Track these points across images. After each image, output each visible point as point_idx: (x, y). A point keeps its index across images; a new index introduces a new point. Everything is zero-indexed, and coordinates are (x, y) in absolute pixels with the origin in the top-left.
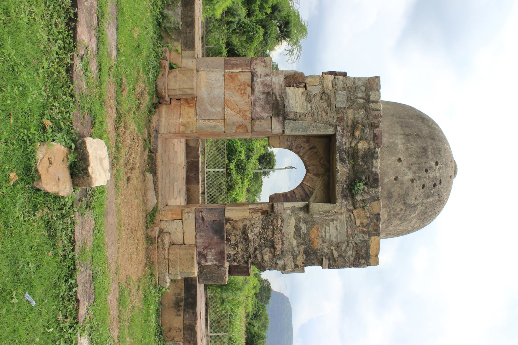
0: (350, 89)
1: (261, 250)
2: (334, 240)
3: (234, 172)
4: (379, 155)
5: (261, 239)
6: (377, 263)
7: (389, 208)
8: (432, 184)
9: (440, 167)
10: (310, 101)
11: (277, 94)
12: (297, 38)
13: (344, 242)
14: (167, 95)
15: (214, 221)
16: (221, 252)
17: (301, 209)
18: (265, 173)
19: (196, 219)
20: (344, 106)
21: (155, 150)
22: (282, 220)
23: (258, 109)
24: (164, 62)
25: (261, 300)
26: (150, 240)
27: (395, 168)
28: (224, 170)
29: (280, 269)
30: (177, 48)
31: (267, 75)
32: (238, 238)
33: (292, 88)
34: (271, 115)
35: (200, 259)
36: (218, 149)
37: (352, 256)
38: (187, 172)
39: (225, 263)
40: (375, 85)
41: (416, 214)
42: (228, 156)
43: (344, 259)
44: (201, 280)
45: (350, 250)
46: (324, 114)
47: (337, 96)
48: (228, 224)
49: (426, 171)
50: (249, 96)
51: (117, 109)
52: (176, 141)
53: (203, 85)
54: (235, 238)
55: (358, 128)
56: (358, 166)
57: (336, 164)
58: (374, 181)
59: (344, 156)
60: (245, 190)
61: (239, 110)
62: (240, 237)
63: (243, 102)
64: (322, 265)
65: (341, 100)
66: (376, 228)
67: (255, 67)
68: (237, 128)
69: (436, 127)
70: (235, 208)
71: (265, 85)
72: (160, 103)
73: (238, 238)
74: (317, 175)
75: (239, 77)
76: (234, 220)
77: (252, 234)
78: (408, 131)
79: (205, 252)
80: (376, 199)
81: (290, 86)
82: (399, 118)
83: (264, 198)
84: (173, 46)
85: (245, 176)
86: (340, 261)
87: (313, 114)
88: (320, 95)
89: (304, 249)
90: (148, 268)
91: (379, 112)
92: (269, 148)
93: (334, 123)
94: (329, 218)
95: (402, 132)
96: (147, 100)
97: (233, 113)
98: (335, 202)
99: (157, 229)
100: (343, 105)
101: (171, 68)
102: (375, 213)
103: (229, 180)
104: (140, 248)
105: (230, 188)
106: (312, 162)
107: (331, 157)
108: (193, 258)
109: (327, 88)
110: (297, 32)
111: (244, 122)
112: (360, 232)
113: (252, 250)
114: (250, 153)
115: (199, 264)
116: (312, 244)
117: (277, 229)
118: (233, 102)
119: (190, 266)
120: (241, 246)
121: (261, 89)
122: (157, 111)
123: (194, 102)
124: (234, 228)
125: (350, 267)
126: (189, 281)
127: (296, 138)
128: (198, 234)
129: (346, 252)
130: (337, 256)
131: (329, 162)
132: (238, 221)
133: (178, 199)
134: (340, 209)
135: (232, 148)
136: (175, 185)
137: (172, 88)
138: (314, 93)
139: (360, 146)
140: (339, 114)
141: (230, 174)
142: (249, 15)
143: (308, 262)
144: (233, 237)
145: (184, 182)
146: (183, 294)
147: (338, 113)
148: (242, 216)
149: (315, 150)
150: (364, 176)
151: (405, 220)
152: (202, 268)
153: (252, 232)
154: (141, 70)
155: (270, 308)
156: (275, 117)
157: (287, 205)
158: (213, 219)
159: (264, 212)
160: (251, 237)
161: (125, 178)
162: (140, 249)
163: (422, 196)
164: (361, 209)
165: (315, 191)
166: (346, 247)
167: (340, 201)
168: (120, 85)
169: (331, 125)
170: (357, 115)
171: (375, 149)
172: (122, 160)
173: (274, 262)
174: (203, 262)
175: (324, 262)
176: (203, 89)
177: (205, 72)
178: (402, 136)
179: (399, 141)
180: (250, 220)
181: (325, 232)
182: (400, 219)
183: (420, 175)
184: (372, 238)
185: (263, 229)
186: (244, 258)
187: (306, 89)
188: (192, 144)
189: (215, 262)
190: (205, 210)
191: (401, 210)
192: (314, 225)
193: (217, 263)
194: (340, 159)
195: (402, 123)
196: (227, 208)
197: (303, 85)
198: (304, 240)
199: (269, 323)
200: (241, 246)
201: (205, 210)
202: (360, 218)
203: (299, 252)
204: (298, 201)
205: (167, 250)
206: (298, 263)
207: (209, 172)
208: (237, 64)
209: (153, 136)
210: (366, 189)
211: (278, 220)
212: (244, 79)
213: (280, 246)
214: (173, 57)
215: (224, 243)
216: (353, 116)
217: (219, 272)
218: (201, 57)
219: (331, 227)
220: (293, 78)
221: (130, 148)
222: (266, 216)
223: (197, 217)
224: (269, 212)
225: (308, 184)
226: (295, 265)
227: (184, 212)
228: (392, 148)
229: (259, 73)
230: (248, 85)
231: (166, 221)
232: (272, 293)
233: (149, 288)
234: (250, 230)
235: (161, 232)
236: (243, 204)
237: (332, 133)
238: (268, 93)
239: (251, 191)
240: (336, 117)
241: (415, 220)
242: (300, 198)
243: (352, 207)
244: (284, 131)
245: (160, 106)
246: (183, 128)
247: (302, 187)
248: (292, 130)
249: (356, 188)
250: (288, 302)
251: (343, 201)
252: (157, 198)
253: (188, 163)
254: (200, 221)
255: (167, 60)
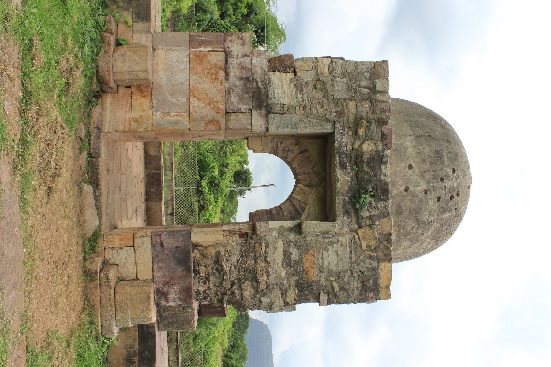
0: (351, 76)
1: (240, 284)
2: (334, 268)
3: (206, 190)
4: (389, 159)
5: (239, 269)
6: (388, 296)
7: (399, 226)
8: (449, 196)
9: (457, 175)
10: (301, 90)
11: (259, 80)
12: (275, 44)
13: (347, 271)
14: (111, 79)
15: (177, 247)
16: (187, 289)
17: (291, 229)
18: (241, 193)
19: (153, 245)
20: (344, 96)
21: (96, 153)
22: (267, 244)
23: (234, 99)
24: (107, 35)
25: (239, 330)
26: (88, 275)
27: (405, 176)
28: (195, 187)
29: (265, 308)
30: (126, 19)
31: (246, 55)
32: (209, 269)
33: (277, 74)
34: (250, 107)
35: (159, 299)
36: (189, 165)
37: (357, 288)
38: (146, 186)
39: (192, 304)
40: (382, 71)
41: (430, 233)
42: (200, 173)
43: (348, 292)
44: (161, 326)
45: (354, 281)
46: (319, 107)
47: (335, 84)
48: (196, 251)
49: (442, 180)
50: (222, 83)
51: (23, 84)
52: (129, 145)
53: (161, 67)
54: (205, 269)
55: (362, 125)
56: (363, 173)
57: (335, 171)
58: (382, 192)
59: (345, 160)
60: (219, 210)
61: (208, 100)
62: (212, 268)
63: (214, 90)
64: (319, 302)
65: (340, 89)
66: (386, 252)
67: (229, 46)
68: (206, 124)
69: (450, 127)
70: (204, 229)
71: (242, 68)
72: (103, 92)
73: (209, 269)
74: (309, 186)
75: (209, 57)
76: (204, 245)
77: (227, 264)
78: (419, 132)
79: (165, 289)
80: (385, 215)
81: (275, 71)
82: (407, 116)
83: (242, 216)
84: (120, 16)
85: (220, 194)
86: (343, 295)
87: (306, 107)
88: (313, 82)
89: (296, 281)
90: (86, 315)
91: (388, 105)
92: (245, 166)
93: (331, 119)
94: (327, 240)
95: (411, 133)
96: (79, 82)
97: (201, 104)
98: (334, 220)
99: (99, 261)
100: (343, 95)
101: (118, 44)
102: (385, 233)
103: (200, 199)
104: (72, 287)
105: (202, 208)
106: (303, 169)
107: (328, 164)
108: (149, 298)
109: (322, 74)
110: (275, 37)
111: (215, 117)
112: (366, 258)
113: (228, 284)
114: (225, 169)
115: (158, 305)
116: (306, 274)
117: (260, 256)
118: (201, 91)
119: (145, 310)
120: (213, 280)
121: (238, 74)
122: (100, 101)
123: (149, 90)
124: (203, 256)
125: (354, 303)
126: (145, 328)
127: (283, 139)
128: (155, 265)
129: (350, 284)
130: (338, 289)
131: (324, 169)
132: (208, 246)
133: (134, 220)
134: (341, 229)
135: (204, 163)
136: (129, 202)
137: (119, 70)
138: (306, 80)
139: (365, 147)
140: (338, 107)
141: (202, 192)
142: (223, 16)
143: (302, 299)
144: (202, 267)
145: (143, 200)
146: (137, 347)
147: (337, 105)
148: (214, 240)
149: (307, 154)
150: (369, 186)
151: (417, 241)
152: (162, 311)
153: (227, 260)
154: (70, 39)
155: (248, 338)
156: (256, 110)
157: (273, 224)
158: (176, 244)
159: (243, 235)
160: (226, 267)
161: (43, 189)
162: (73, 289)
163: (437, 210)
164: (368, 228)
165: (308, 207)
166: (350, 277)
167: (341, 218)
168: (29, 47)
169: (328, 121)
170: (360, 109)
171: (383, 151)
172: (34, 161)
173: (257, 300)
174: (163, 302)
175: (321, 297)
176: (161, 73)
177: (164, 51)
178: (412, 138)
179: (409, 144)
180: (225, 246)
181: (322, 258)
182: (411, 240)
183: (435, 185)
184: (382, 265)
185: (242, 256)
186: (217, 295)
187: (295, 75)
188: (152, 152)
189: (179, 303)
190: (165, 233)
191: (413, 228)
192: (308, 250)
193: (181, 303)
194: (340, 164)
195: (411, 121)
196: (195, 230)
197: (292, 69)
198: (295, 270)
199: (248, 353)
200: (213, 280)
201: (165, 233)
202: (367, 238)
203: (290, 285)
204: (285, 220)
205: (113, 288)
206: (288, 300)
207: (178, 190)
208: (206, 41)
209: (93, 135)
210: (373, 202)
211: (261, 245)
212: (215, 61)
213: (265, 279)
214: (122, 31)
215: (190, 277)
216: (355, 110)
217: (185, 315)
218: (160, 31)
219: (330, 252)
220: (279, 60)
221: (48, 145)
222: (246, 240)
223: (154, 243)
224: (249, 234)
225: (299, 198)
226: (285, 302)
227: (136, 236)
228: (401, 153)
229: (235, 53)
230: (221, 68)
231: (113, 248)
232: (250, 322)
233: (87, 342)
234: (225, 259)
235: (105, 264)
236: (216, 225)
237: (329, 131)
238: (247, 79)
239: (225, 211)
240: (334, 111)
241: (428, 240)
242: (289, 216)
243: (356, 226)
244: (267, 129)
245: (104, 95)
246: (134, 125)
247: (291, 201)
248: (278, 127)
249: (361, 201)
250: (268, 330)
251: (345, 218)
252: (100, 218)
253: (147, 175)
254: (159, 248)
255: (112, 34)
